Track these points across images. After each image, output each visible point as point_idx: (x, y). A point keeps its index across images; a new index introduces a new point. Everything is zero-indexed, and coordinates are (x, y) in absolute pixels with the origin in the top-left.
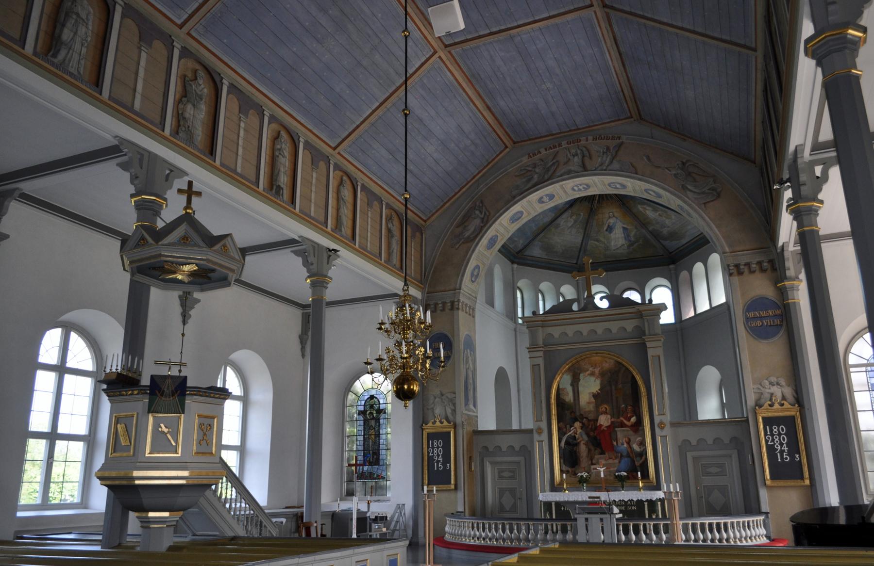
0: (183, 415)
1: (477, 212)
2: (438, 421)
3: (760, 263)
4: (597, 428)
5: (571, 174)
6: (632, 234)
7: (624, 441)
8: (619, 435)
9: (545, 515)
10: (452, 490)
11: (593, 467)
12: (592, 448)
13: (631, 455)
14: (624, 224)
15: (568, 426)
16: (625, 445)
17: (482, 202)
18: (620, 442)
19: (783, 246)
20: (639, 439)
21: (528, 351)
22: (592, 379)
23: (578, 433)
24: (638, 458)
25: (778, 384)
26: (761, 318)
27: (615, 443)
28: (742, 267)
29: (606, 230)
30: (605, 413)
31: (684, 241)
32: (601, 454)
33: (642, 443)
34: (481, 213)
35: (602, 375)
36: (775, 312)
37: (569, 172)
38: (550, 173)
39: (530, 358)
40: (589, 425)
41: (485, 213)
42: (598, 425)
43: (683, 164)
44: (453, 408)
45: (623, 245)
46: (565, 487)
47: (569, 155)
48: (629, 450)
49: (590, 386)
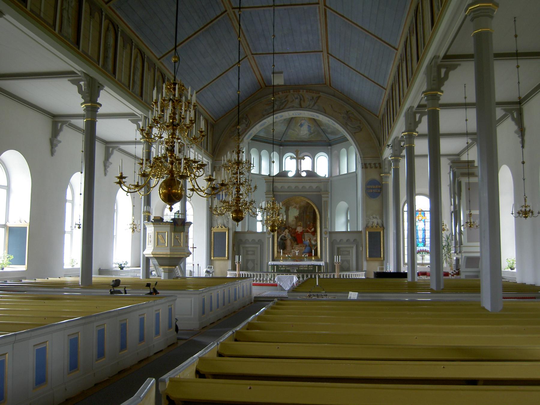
0: (147, 221)
1: (244, 121)
2: (220, 226)
3: (375, 164)
4: (296, 233)
5: (293, 108)
6: (313, 129)
7: (308, 239)
8: (306, 237)
9: (271, 271)
10: (226, 260)
11: (292, 250)
12: (293, 242)
13: (310, 246)
14: (309, 124)
15: (282, 231)
16: (308, 241)
17: (247, 115)
18: (306, 239)
19: (385, 159)
20: (315, 238)
21: (265, 194)
22: (295, 210)
23: (287, 235)
24: (313, 247)
25: (376, 218)
26: (373, 189)
27: (304, 240)
28: (367, 165)
29: (299, 126)
30: (300, 226)
31: (337, 137)
32: (297, 245)
33: (316, 240)
34: (246, 121)
35: (300, 208)
36: (377, 190)
37: (293, 107)
38: (283, 105)
39: (266, 197)
40: (292, 231)
41: (248, 122)
42: (296, 231)
43: (347, 112)
44: (227, 220)
45: (306, 134)
46: (281, 259)
47: (293, 98)
48: (310, 243)
49: (294, 213)
